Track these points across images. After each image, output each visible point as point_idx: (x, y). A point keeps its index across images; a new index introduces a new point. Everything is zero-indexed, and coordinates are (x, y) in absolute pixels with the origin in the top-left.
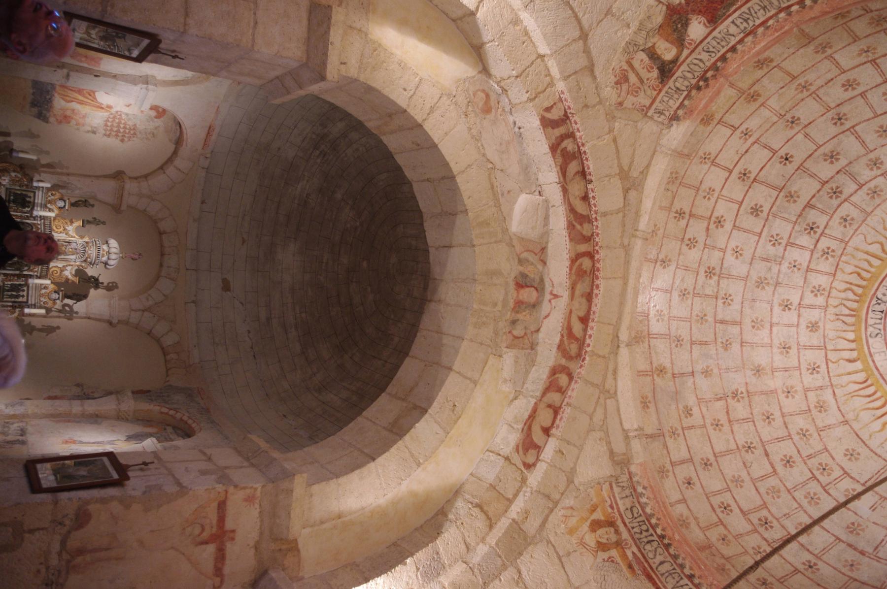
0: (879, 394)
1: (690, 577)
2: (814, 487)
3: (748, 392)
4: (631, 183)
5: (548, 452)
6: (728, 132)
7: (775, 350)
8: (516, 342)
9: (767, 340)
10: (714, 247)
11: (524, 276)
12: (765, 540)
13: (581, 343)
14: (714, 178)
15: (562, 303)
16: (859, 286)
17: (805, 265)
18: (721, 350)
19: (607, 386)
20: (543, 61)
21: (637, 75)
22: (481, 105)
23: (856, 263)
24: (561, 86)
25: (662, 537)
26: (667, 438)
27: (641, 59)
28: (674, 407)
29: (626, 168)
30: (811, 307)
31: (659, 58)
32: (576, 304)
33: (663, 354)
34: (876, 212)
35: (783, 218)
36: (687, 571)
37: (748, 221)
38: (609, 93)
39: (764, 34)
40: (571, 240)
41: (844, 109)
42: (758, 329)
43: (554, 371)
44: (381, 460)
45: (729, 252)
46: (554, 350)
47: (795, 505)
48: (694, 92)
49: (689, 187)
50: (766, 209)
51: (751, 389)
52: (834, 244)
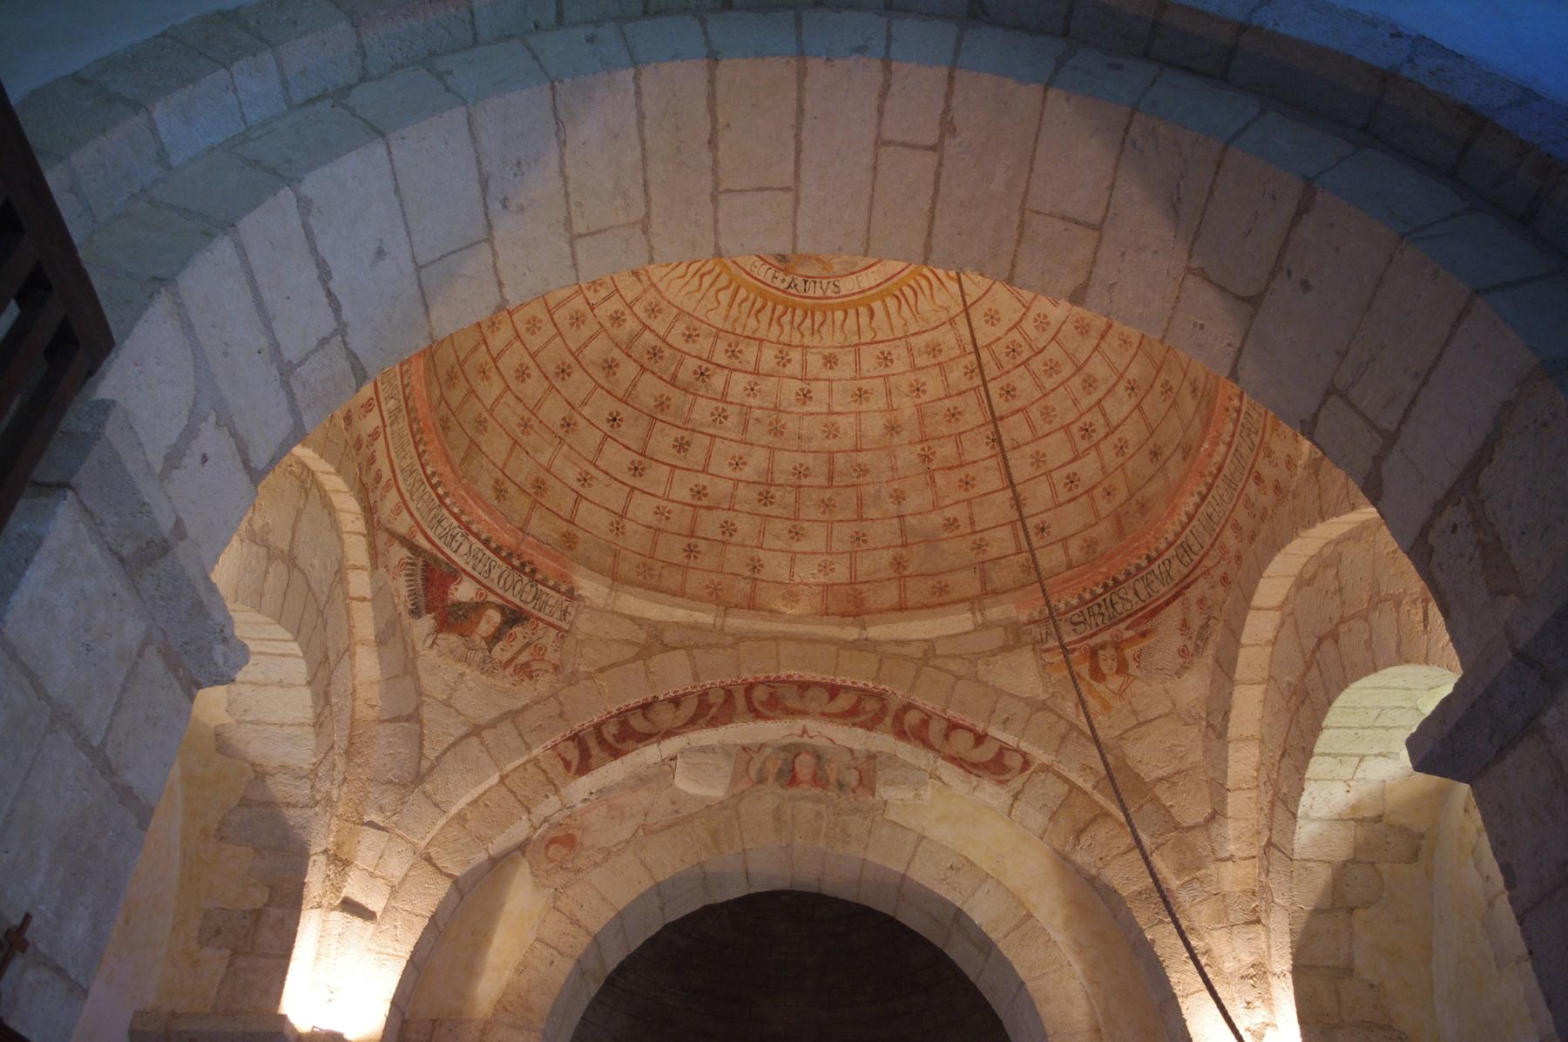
0: (912, 283)
1: (1150, 560)
2: (1037, 364)
3: (921, 441)
4: (655, 641)
5: (1009, 739)
6: (584, 504)
7: (864, 407)
8: (866, 781)
9: (852, 419)
10: (733, 496)
11: (780, 775)
12: (1107, 435)
13: (865, 694)
14: (643, 510)
15: (812, 725)
16: (774, 310)
17: (750, 377)
18: (868, 478)
19: (920, 655)
20: (507, 776)
21: (519, 652)
22: (565, 851)
23: (744, 316)
24: (537, 751)
25: (1105, 586)
26: (986, 557)
27: (500, 652)
28: (945, 545)
29: (636, 650)
30: (804, 365)
31: (499, 629)
32: (813, 707)
33: (876, 562)
34: (678, 303)
35: (691, 410)
36: (1144, 563)
37: (697, 453)
38: (543, 685)
39: (470, 514)
40: (730, 721)
41: (551, 369)
42: (837, 430)
43: (901, 734)
44: (1022, 973)
45: (737, 475)
46: (873, 734)
47: (1061, 389)
48: (539, 576)
49: (655, 543)
50: (679, 433)
51: (918, 437)
52: (722, 345)
